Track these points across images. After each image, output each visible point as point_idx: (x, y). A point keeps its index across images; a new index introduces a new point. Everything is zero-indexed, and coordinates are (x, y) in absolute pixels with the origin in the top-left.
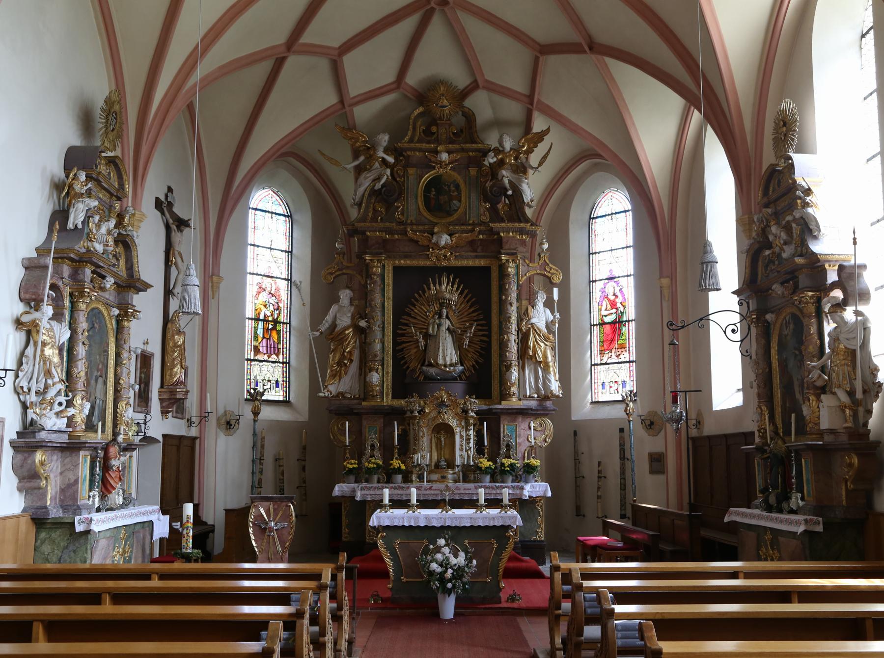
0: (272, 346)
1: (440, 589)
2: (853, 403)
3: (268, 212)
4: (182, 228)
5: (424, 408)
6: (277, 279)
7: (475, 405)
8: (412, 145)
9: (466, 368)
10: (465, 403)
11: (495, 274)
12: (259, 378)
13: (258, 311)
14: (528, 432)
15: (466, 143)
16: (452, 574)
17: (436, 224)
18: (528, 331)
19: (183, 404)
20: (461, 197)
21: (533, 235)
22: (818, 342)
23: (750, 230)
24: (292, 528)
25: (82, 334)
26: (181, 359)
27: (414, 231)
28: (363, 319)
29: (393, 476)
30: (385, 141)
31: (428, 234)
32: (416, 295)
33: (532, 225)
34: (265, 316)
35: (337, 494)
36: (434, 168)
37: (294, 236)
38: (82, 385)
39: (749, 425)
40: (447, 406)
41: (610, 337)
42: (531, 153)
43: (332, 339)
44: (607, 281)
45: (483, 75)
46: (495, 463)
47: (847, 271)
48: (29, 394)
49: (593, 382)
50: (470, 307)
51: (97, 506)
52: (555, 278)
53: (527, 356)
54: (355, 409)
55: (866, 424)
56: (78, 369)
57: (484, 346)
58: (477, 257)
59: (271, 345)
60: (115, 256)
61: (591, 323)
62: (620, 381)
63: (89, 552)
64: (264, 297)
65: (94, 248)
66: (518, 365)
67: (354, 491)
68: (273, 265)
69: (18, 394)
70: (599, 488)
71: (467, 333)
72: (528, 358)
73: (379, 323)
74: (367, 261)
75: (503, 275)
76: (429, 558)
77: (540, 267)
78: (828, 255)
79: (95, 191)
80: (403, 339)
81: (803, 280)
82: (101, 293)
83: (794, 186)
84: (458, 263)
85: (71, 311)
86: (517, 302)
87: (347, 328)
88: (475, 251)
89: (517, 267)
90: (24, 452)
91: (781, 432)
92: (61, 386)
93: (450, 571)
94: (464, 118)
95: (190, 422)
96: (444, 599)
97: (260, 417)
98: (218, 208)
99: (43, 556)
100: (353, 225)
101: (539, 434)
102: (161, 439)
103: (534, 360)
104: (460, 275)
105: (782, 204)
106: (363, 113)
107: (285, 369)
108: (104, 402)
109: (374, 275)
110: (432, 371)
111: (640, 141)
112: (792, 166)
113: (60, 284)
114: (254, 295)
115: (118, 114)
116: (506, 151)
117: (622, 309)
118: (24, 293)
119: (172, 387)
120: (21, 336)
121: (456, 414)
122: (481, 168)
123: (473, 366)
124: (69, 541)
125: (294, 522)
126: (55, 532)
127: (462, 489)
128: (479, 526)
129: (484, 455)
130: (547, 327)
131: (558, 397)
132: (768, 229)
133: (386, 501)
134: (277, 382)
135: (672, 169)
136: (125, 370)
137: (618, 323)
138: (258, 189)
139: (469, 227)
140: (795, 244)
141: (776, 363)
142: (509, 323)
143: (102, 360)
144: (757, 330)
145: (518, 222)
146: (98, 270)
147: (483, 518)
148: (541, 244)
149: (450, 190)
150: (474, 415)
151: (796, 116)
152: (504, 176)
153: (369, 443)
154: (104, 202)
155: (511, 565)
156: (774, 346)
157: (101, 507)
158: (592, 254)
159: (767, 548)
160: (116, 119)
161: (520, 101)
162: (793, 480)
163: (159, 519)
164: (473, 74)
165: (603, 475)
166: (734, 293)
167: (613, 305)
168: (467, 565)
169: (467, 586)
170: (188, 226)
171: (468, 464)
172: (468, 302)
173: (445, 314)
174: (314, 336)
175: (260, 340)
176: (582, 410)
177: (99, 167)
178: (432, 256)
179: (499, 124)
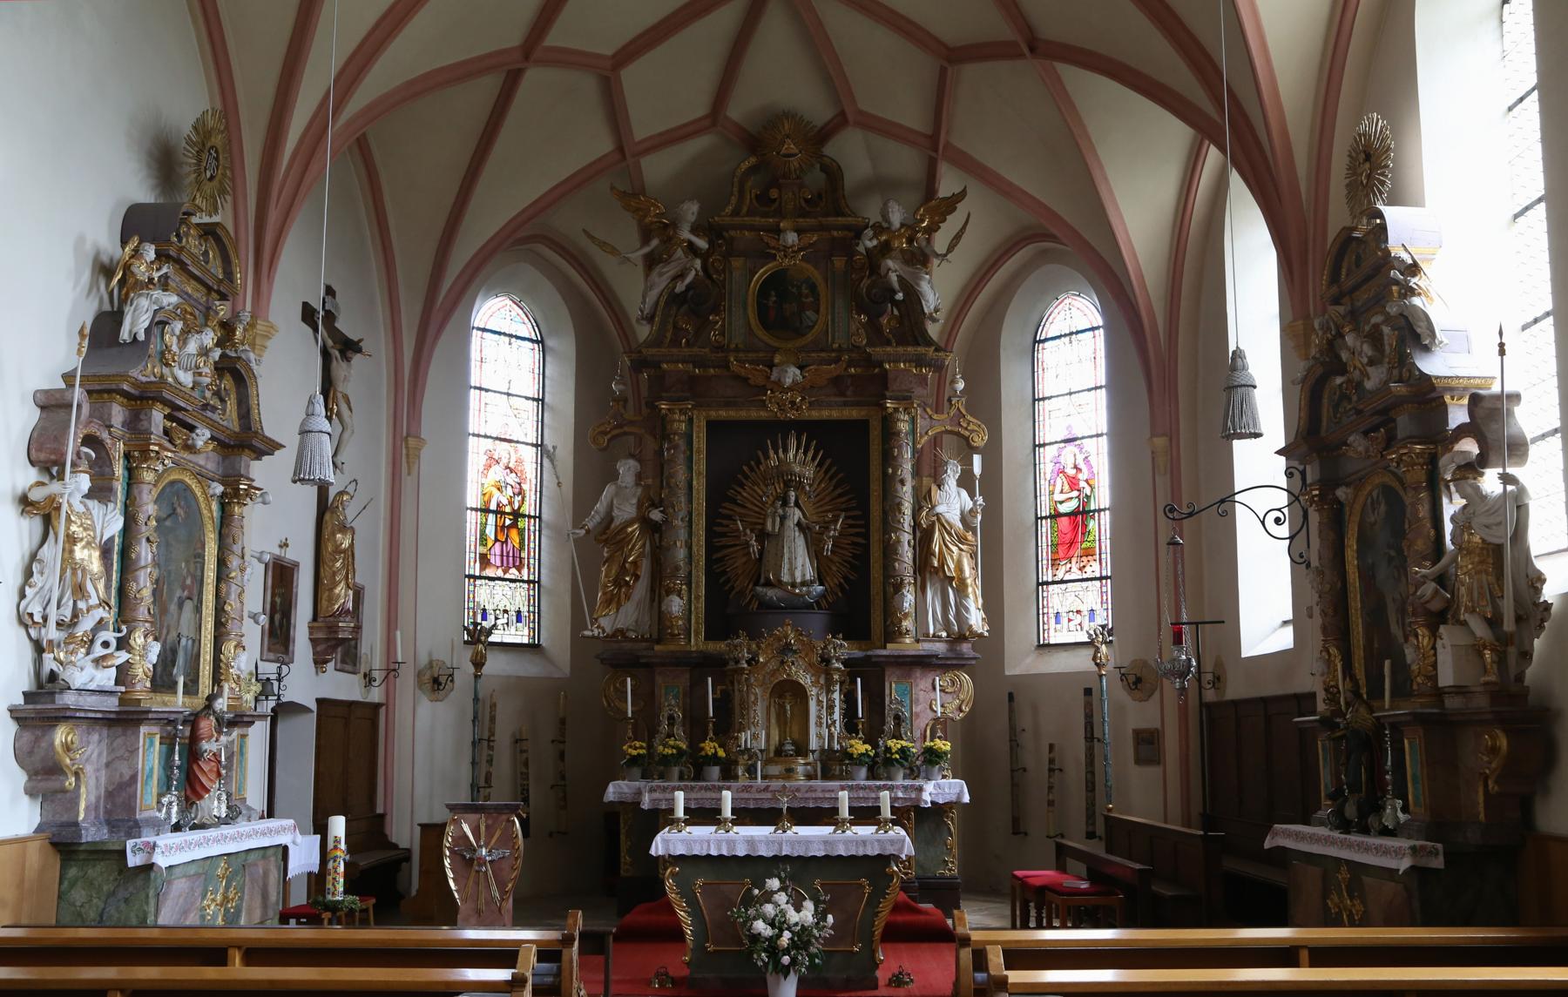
0: (511, 554)
1: (770, 967)
2: (1498, 640)
3: (505, 334)
4: (349, 354)
5: (758, 655)
6: (518, 445)
7: (843, 649)
8: (737, 220)
10: (825, 647)
11: (876, 433)
12: (490, 608)
13: (487, 496)
14: (932, 695)
15: (827, 215)
16: (791, 939)
17: (775, 350)
18: (932, 526)
19: (356, 648)
21: (939, 368)
22: (1432, 532)
23: (1307, 344)
24: (516, 859)
25: (146, 524)
26: (347, 574)
27: (741, 362)
29: (706, 768)
32: (745, 468)
34: (498, 505)
35: (611, 799)
36: (774, 257)
38: (146, 612)
39: (1308, 680)
40: (795, 652)
41: (1068, 538)
42: (936, 231)
43: (606, 542)
44: (1062, 445)
46: (875, 746)
47: (1486, 404)
48: (45, 626)
49: (1041, 612)
50: (835, 488)
51: (174, 820)
52: (976, 439)
53: (928, 569)
55: (1520, 678)
56: (138, 584)
58: (845, 404)
59: (508, 553)
60: (217, 394)
62: (1085, 609)
63: (152, 902)
64: (497, 473)
65: (175, 379)
66: (915, 584)
67: (639, 793)
68: (513, 421)
69: (26, 627)
70: (1050, 788)
73: (682, 514)
74: (663, 411)
75: (889, 434)
76: (752, 912)
77: (951, 420)
78: (1449, 377)
79: (176, 279)
80: (724, 541)
81: (1404, 424)
82: (186, 455)
83: (1387, 260)
84: (815, 415)
85: (129, 485)
86: (913, 478)
87: (630, 523)
88: (842, 394)
89: (913, 421)
90: (35, 727)
91: (1364, 691)
92: (109, 616)
93: (787, 935)
94: (823, 176)
95: (369, 679)
96: (778, 983)
97: (486, 670)
98: (417, 322)
99: (73, 909)
100: (640, 352)
101: (949, 698)
102: (313, 706)
103: (941, 574)
104: (818, 434)
105: (1363, 296)
106: (658, 169)
107: (531, 592)
108: (197, 642)
109: (675, 434)
110: (771, 593)
111: (1117, 208)
112: (1383, 228)
113: (105, 435)
114: (481, 470)
115: (220, 151)
116: (893, 228)
117: (1087, 491)
118: (37, 450)
119: (331, 619)
120: (33, 525)
121: (811, 665)
124: (116, 884)
125: (522, 848)
126: (94, 866)
127: (819, 790)
128: (840, 856)
129: (857, 734)
130: (963, 520)
131: (981, 635)
132: (1339, 341)
133: (680, 813)
134: (519, 613)
135: (1171, 245)
136: (234, 587)
137: (1081, 515)
138: (487, 297)
139: (833, 355)
140: (1389, 363)
141: (1354, 573)
142: (900, 513)
143: (192, 570)
144: (1321, 516)
145: (913, 345)
146: (180, 415)
147: (847, 842)
148: (953, 382)
151: (1389, 142)
152: (889, 269)
153: (665, 713)
154: (195, 300)
155: (900, 918)
156: (1350, 543)
157: (182, 822)
158: (1039, 400)
159: (1340, 896)
160: (217, 159)
162: (1388, 777)
163: (294, 843)
165: (1056, 767)
166: (1279, 452)
167: (1073, 483)
168: (817, 923)
169: (817, 961)
170: (359, 350)
172: (831, 479)
173: (793, 499)
174: (576, 536)
175: (490, 544)
176: (1020, 663)
177: (184, 240)
178: (771, 402)
179: (883, 186)
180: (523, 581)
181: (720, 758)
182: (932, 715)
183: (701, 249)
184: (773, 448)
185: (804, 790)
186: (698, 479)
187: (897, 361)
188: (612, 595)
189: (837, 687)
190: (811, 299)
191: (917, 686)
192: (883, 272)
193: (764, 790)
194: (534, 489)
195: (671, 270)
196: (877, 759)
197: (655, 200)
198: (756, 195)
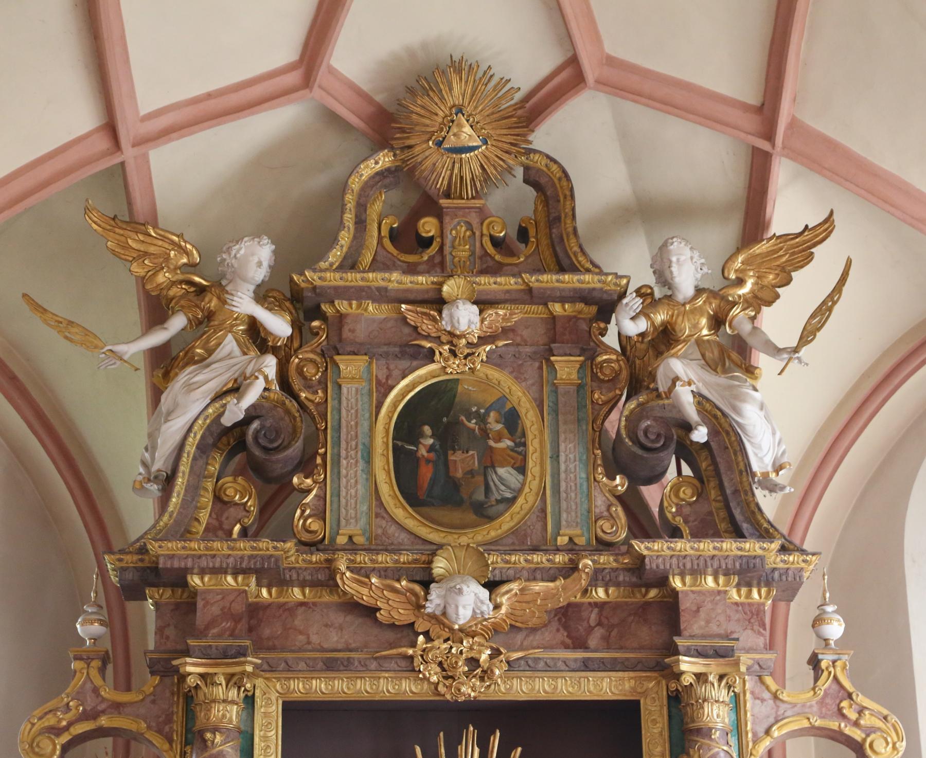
8: (353, 278)
27: (361, 572)
30: (260, 264)
33: (783, 549)
36: (430, 356)
42: (769, 303)
45: (597, 39)
58: (586, 666)
88: (580, 644)
89: (737, 703)
94: (531, 192)
100: (143, 550)
109: (215, 730)
116: (680, 297)
122: (593, 358)
139: (559, 558)
149: (485, 433)
152: (676, 379)
161: (727, 125)
164: (566, 36)
183: (276, 338)
187: (697, 572)
197: (180, 236)
198: (392, 230)
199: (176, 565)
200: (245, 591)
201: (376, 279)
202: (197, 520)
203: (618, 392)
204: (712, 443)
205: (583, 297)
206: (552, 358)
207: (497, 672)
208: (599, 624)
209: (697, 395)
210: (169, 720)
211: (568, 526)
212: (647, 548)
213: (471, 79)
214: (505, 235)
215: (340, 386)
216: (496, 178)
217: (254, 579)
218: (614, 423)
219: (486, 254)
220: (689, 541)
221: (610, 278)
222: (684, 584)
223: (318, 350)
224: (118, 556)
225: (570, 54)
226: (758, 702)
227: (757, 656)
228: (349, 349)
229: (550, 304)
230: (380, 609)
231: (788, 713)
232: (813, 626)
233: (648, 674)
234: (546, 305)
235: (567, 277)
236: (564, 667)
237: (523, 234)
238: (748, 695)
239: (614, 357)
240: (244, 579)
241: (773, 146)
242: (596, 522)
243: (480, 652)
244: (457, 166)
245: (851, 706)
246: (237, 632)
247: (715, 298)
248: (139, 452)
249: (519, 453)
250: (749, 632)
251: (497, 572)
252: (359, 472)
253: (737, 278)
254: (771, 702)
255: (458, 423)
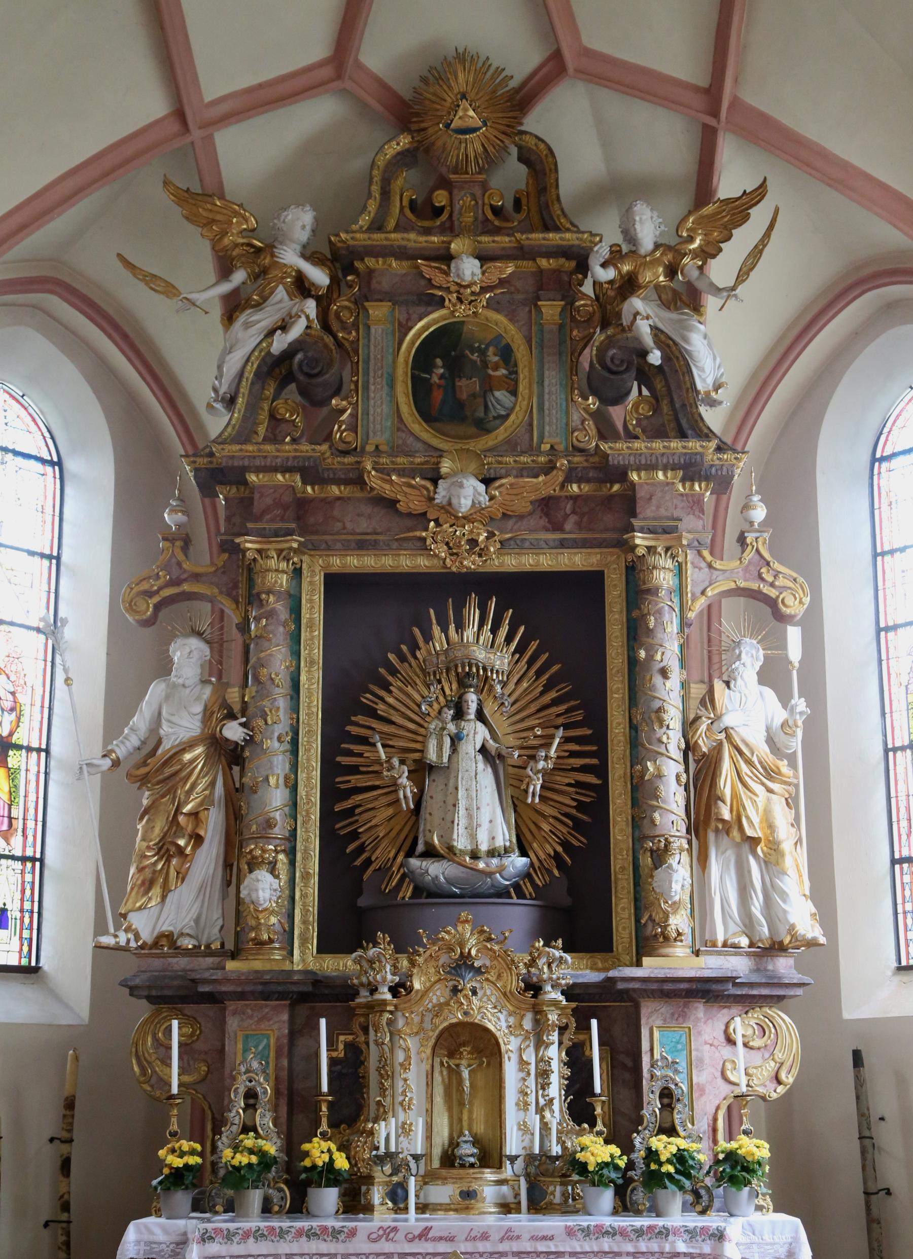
8: (378, 238)
9: (537, 864)
10: (532, 963)
20: (516, 382)
21: (722, 484)
28: (235, 718)
29: (312, 1192)
30: (303, 227)
31: (423, 478)
32: (391, 657)
33: (719, 449)
36: (440, 303)
37: (65, 516)
40: (478, 971)
42: (714, 256)
46: (627, 1148)
49: (900, 909)
50: (547, 689)
52: (790, 601)
53: (713, 824)
54: (206, 981)
57: (588, 800)
61: (886, 744)
66: (690, 851)
71: (537, 762)
72: (717, 830)
73: (282, 727)
77: (746, 570)
80: (356, 780)
88: (557, 527)
89: (680, 571)
94: (523, 169)
100: (211, 454)
103: (735, 833)
107: (28, 878)
109: (268, 593)
116: (642, 251)
123: (557, 857)
127: (526, 1236)
129: (593, 1124)
148: (747, 507)
149: (485, 364)
150: (561, 998)
152: (637, 313)
161: (681, 105)
171: (545, 1154)
172: (539, 674)
173: (473, 707)
180: (13, 858)
181: (339, 1172)
182: (725, 1089)
183: (318, 288)
184: (439, 624)
185: (495, 1236)
186: (309, 672)
188: (154, 872)
189: (555, 1037)
190: (504, 372)
191: (699, 1033)
192: (626, 320)
193: (420, 1236)
194: (38, 704)
195: (265, 318)
196: (631, 1173)
197: (241, 206)
199: (236, 464)
200: (293, 487)
201: (396, 237)
202: (256, 433)
203: (592, 331)
204: (665, 368)
205: (564, 252)
206: (539, 303)
207: (492, 549)
208: (574, 512)
209: (655, 329)
210: (236, 586)
211: (550, 436)
212: (611, 448)
213: (473, 68)
214: (503, 204)
215: (369, 327)
216: (495, 156)
217: (298, 477)
218: (587, 358)
219: (487, 220)
220: (644, 441)
221: (586, 236)
222: (640, 478)
223: (353, 299)
224: (192, 459)
225: (555, 47)
226: (697, 570)
227: (697, 535)
228: (376, 297)
229: (538, 260)
230: (399, 501)
231: (720, 578)
232: (742, 512)
233: (610, 550)
234: (534, 260)
235: (551, 235)
236: (544, 546)
237: (517, 204)
238: (689, 564)
239: (589, 302)
240: (290, 476)
241: (719, 122)
242: (572, 433)
243: (479, 534)
244: (463, 145)
245: (768, 572)
246: (286, 518)
247: (670, 251)
248: (209, 378)
249: (512, 379)
250: (691, 516)
251: (492, 471)
252: (384, 396)
253: (688, 236)
254: (707, 570)
255: (464, 356)
